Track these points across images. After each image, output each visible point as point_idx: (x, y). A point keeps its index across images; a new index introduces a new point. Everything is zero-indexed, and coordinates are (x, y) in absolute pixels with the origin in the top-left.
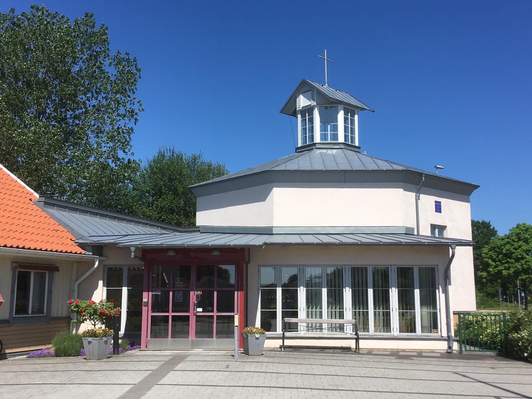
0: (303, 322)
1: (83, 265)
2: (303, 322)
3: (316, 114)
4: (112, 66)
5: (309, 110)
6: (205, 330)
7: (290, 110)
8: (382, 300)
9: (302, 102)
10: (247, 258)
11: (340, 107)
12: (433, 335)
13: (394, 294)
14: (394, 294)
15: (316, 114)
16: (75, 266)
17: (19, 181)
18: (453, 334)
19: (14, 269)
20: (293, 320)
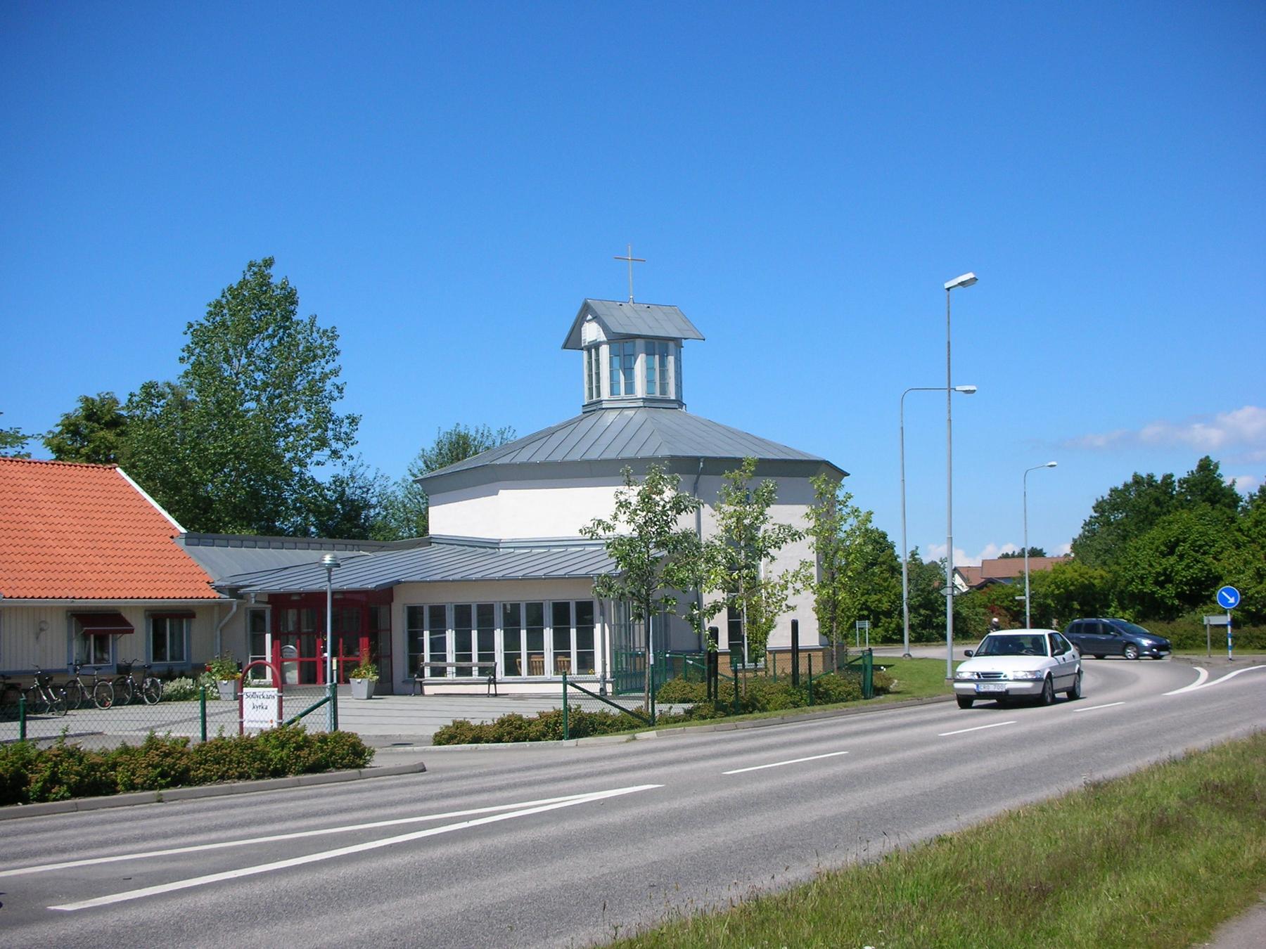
0: (451, 665)
1: (223, 608)
2: (451, 665)
3: (605, 351)
4: (307, 321)
5: (597, 345)
6: (1163, 619)
7: (573, 341)
8: (536, 643)
9: (591, 332)
10: (170, 687)
11: (640, 343)
12: (589, 677)
13: (548, 634)
14: (548, 634)
15: (605, 351)
16: (216, 608)
17: (165, 514)
18: (608, 676)
19: (147, 618)
20: (441, 664)
